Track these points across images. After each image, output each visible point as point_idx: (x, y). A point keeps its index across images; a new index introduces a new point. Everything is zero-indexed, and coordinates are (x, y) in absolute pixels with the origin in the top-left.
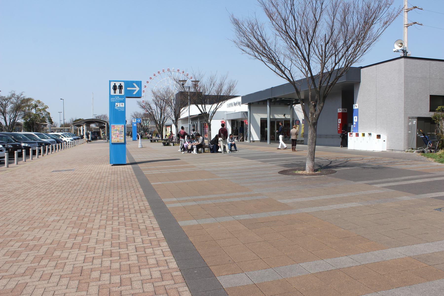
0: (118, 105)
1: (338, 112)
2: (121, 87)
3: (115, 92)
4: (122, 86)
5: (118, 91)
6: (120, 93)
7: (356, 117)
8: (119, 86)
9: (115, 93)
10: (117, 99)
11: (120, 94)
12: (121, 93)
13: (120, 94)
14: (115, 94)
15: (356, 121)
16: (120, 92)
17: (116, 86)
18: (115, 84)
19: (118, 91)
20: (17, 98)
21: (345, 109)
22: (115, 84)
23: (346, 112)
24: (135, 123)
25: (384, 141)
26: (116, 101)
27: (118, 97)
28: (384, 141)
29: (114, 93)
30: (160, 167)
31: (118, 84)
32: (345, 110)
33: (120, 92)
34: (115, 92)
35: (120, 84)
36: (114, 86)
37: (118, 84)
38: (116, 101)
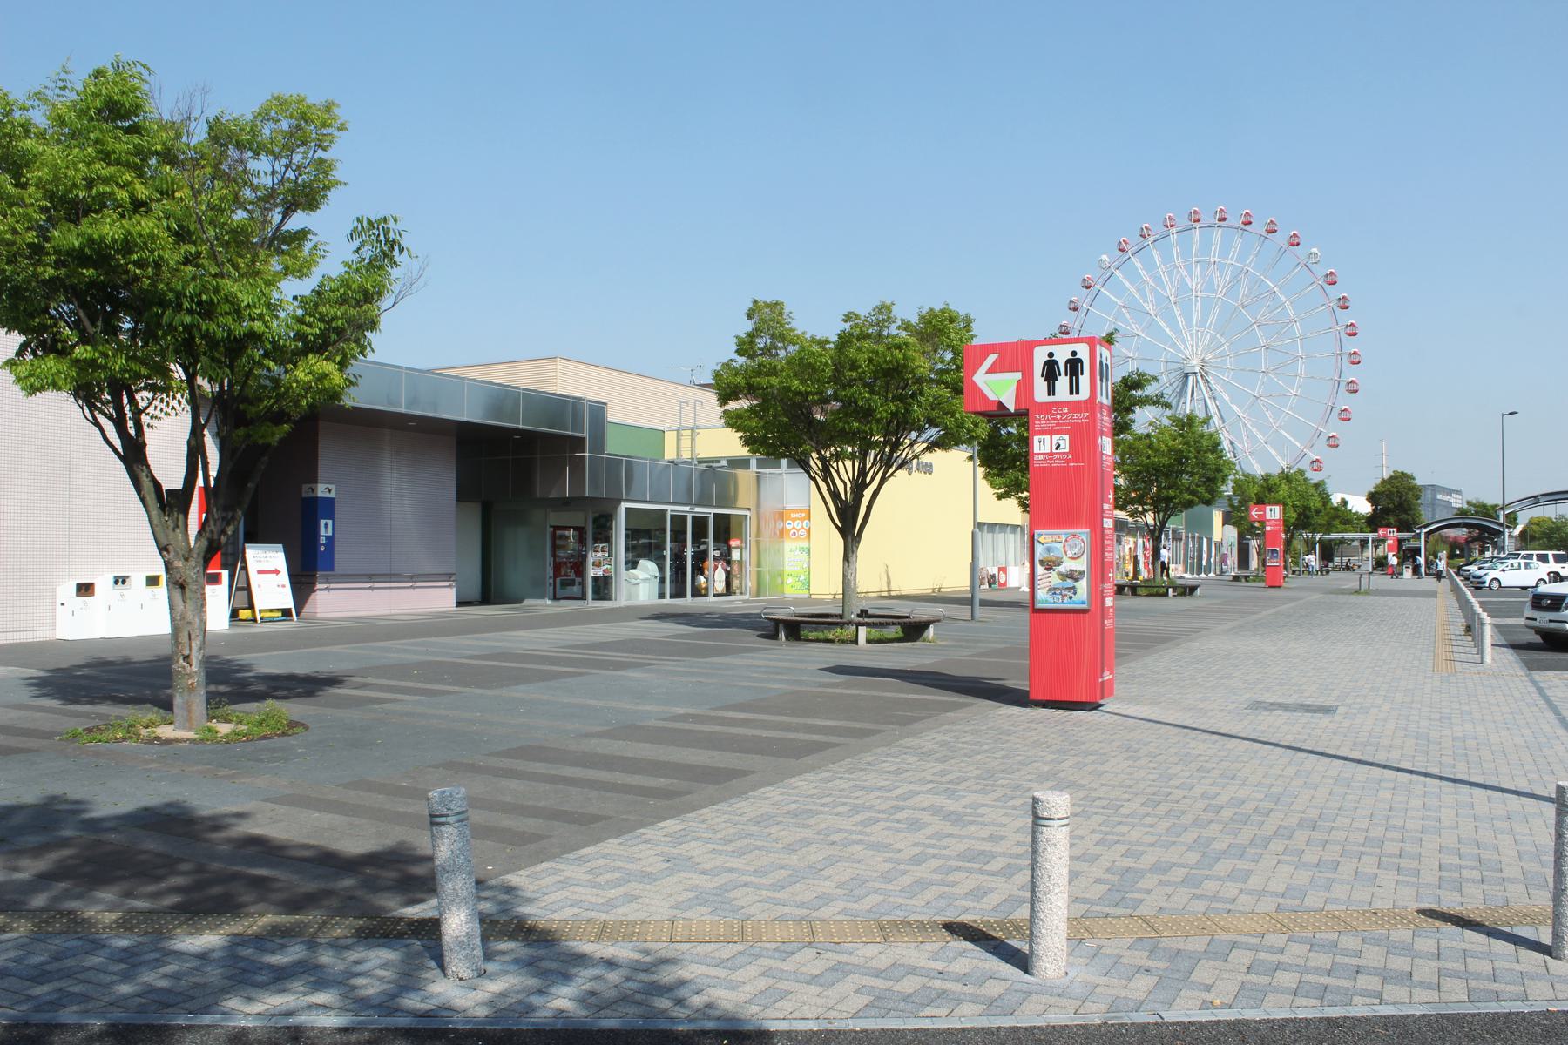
0: (1062, 443)
1: (304, 495)
2: (1074, 365)
3: (1051, 391)
4: (1080, 361)
5: (1063, 382)
6: (1071, 393)
7: (330, 522)
8: (1068, 361)
9: (1054, 394)
10: (1059, 416)
11: (1075, 398)
12: (1077, 393)
13: (1075, 398)
14: (1051, 399)
15: (330, 533)
16: (1074, 388)
17: (1056, 363)
18: (1051, 355)
19: (1063, 382)
20: (237, 426)
21: (330, 486)
22: (1051, 355)
23: (332, 495)
24: (1276, 520)
25: (62, 604)
26: (1058, 425)
27: (1066, 410)
28: (62, 604)
29: (1049, 395)
30: (910, 696)
31: (1062, 354)
32: (330, 491)
33: (1074, 388)
34: (1051, 391)
35: (1074, 353)
36: (1046, 363)
37: (1062, 354)
38: (1058, 425)
